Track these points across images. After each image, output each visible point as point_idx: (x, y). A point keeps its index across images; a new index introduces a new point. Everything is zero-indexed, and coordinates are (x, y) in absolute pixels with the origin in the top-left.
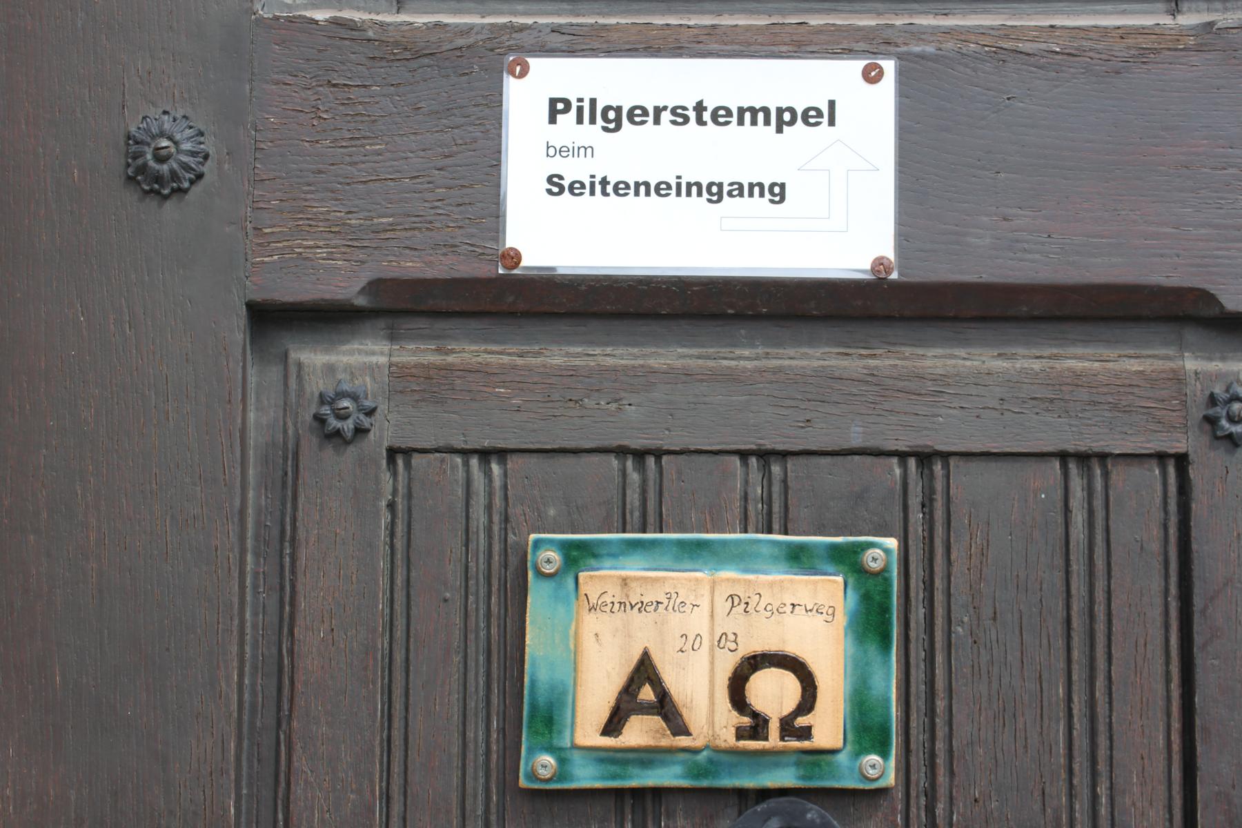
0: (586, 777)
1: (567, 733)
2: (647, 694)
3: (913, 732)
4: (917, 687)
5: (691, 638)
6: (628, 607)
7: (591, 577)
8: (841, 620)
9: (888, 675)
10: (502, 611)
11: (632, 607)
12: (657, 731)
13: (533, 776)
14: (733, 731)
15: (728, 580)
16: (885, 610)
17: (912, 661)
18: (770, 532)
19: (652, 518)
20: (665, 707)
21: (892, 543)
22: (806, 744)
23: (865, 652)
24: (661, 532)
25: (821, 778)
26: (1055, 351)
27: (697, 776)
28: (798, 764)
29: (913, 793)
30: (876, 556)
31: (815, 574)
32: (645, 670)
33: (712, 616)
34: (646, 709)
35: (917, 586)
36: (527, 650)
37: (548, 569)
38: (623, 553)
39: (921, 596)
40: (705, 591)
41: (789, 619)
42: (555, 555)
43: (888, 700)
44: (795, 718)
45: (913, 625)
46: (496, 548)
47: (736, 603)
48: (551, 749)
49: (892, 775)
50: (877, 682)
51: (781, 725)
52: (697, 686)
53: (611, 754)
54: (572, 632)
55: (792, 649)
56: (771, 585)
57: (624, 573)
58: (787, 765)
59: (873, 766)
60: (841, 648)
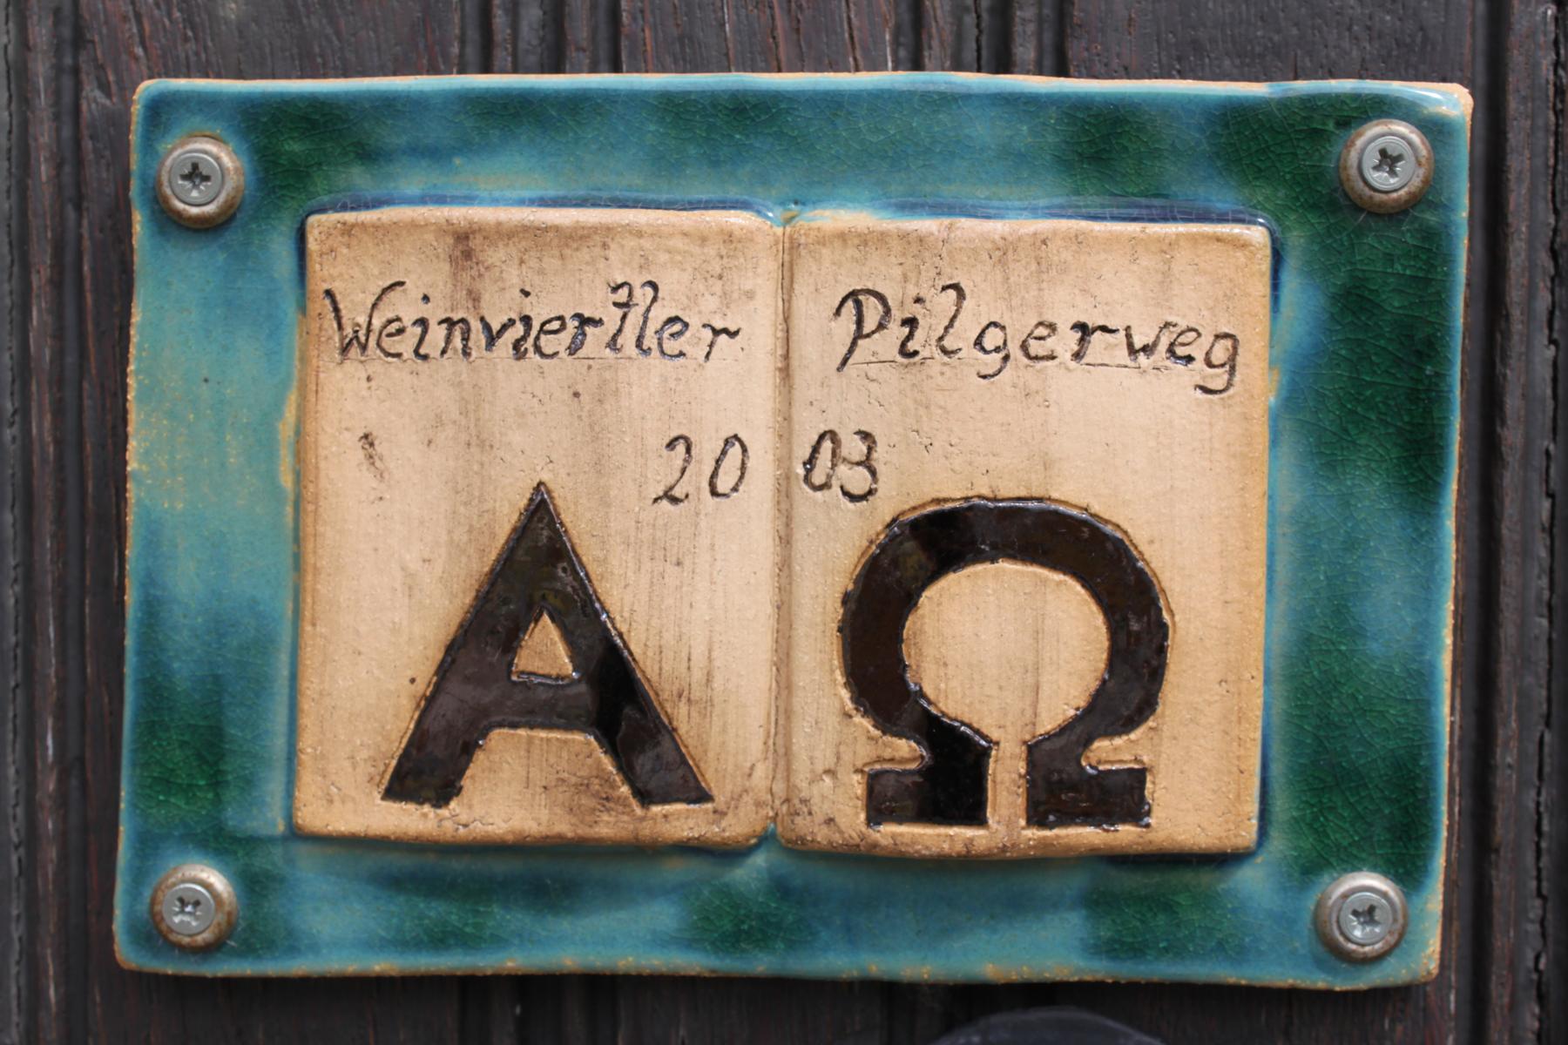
0: (340, 937)
1: (274, 786)
2: (546, 651)
3: (1506, 780)
4: (1522, 626)
5: (706, 450)
6: (478, 337)
7: (348, 230)
8: (1259, 382)
9: (1427, 584)
10: (71, 359)
11: (492, 339)
12: (583, 787)
13: (153, 933)
14: (857, 785)
15: (843, 237)
16: (1422, 348)
17: (1509, 532)
18: (1004, 65)
19: (580, 29)
20: (617, 704)
21: (1452, 100)
22: (1125, 834)
23: (1345, 501)
24: (616, 68)
25: (1176, 950)
26: (977, 738)
27: (733, 940)
28: (1097, 902)
29: (1499, 995)
30: (1395, 146)
31: (1165, 218)
32: (536, 568)
33: (786, 372)
34: (541, 708)
35: (1532, 265)
36: (133, 491)
37: (196, 203)
38: (465, 147)
39: (1543, 301)
40: (762, 280)
41: (1065, 382)
42: (224, 157)
43: (1423, 677)
44: (1088, 741)
45: (1513, 403)
46: (44, 135)
47: (869, 325)
48: (220, 842)
49: (1434, 945)
50: (1385, 609)
51: (1031, 763)
52: (727, 619)
53: (430, 859)
54: (286, 430)
55: (1076, 489)
56: (1003, 252)
57: (458, 214)
58: (1055, 905)
59: (1368, 915)
60: (1258, 486)
